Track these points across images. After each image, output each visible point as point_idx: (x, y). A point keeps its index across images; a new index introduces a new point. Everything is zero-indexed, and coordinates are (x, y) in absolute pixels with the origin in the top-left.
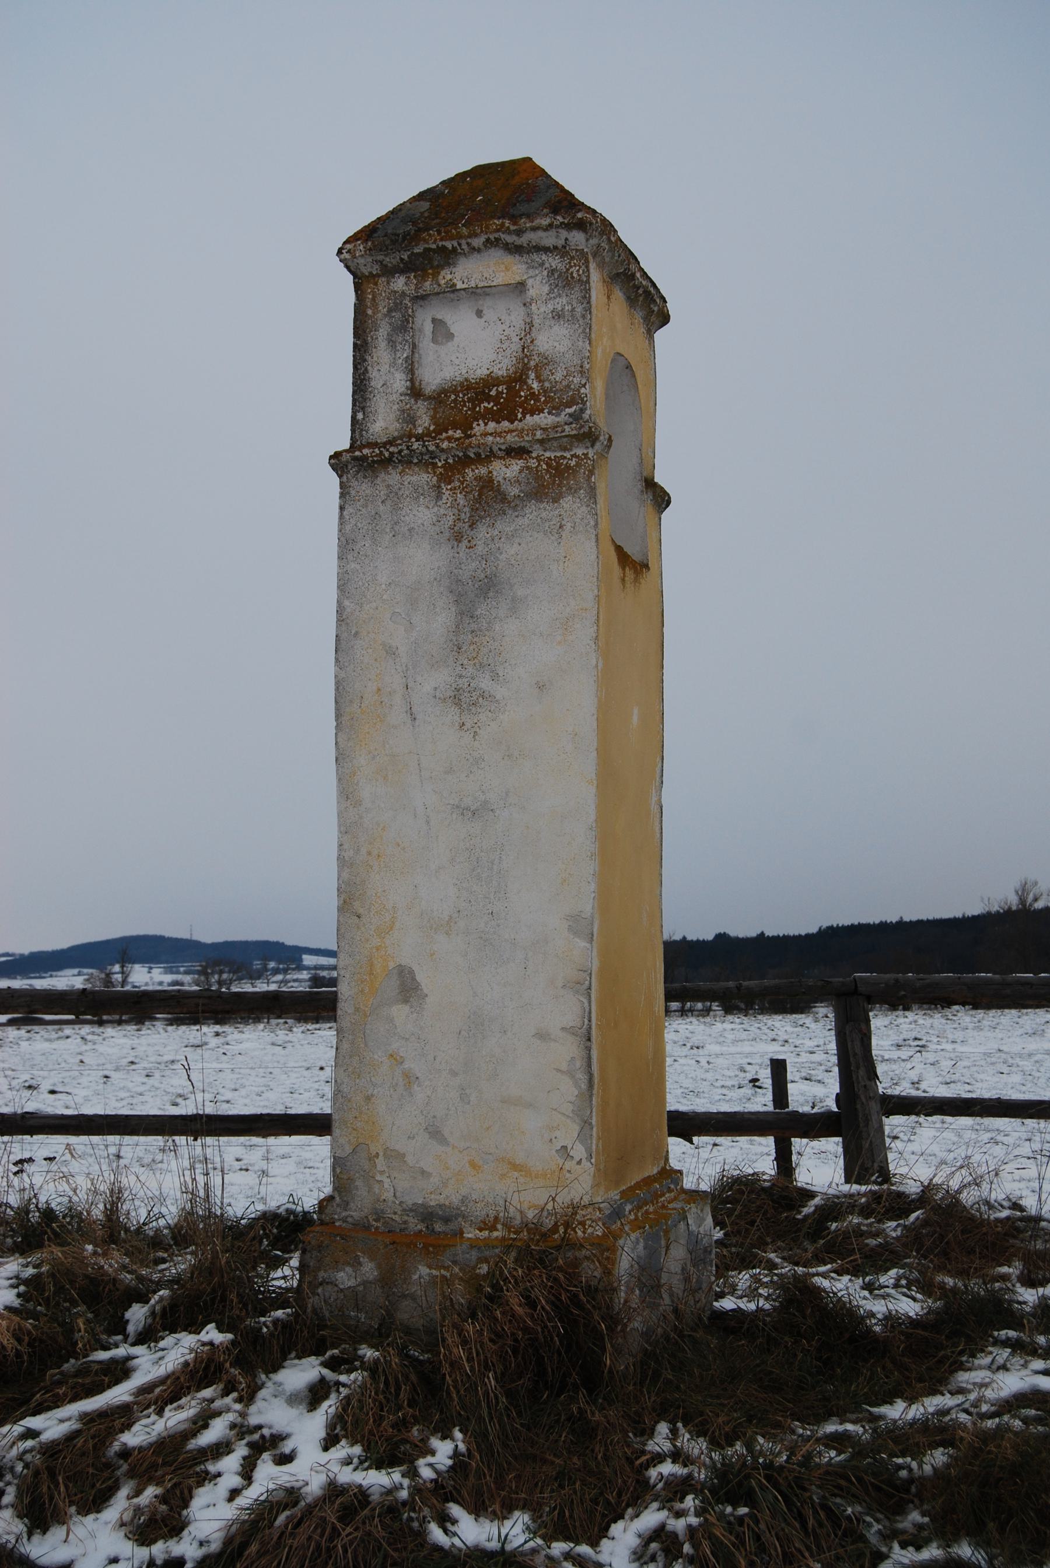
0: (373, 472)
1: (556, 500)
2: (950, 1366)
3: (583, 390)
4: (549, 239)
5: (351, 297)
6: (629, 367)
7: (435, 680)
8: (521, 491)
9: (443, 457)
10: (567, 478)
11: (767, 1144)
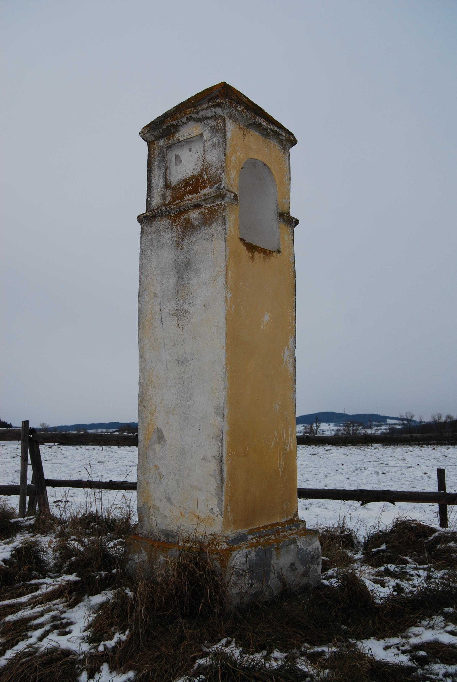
0: (151, 221)
1: (211, 225)
2: (410, 623)
3: (221, 176)
4: (209, 113)
5: (147, 151)
6: (265, 164)
7: (170, 307)
8: (199, 223)
9: (173, 212)
10: (215, 215)
11: (436, 507)
